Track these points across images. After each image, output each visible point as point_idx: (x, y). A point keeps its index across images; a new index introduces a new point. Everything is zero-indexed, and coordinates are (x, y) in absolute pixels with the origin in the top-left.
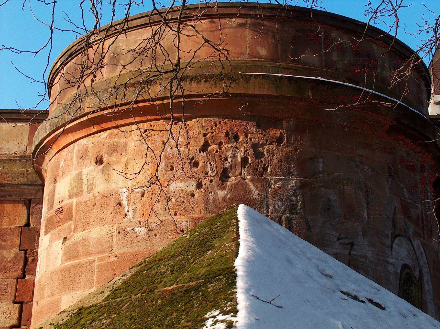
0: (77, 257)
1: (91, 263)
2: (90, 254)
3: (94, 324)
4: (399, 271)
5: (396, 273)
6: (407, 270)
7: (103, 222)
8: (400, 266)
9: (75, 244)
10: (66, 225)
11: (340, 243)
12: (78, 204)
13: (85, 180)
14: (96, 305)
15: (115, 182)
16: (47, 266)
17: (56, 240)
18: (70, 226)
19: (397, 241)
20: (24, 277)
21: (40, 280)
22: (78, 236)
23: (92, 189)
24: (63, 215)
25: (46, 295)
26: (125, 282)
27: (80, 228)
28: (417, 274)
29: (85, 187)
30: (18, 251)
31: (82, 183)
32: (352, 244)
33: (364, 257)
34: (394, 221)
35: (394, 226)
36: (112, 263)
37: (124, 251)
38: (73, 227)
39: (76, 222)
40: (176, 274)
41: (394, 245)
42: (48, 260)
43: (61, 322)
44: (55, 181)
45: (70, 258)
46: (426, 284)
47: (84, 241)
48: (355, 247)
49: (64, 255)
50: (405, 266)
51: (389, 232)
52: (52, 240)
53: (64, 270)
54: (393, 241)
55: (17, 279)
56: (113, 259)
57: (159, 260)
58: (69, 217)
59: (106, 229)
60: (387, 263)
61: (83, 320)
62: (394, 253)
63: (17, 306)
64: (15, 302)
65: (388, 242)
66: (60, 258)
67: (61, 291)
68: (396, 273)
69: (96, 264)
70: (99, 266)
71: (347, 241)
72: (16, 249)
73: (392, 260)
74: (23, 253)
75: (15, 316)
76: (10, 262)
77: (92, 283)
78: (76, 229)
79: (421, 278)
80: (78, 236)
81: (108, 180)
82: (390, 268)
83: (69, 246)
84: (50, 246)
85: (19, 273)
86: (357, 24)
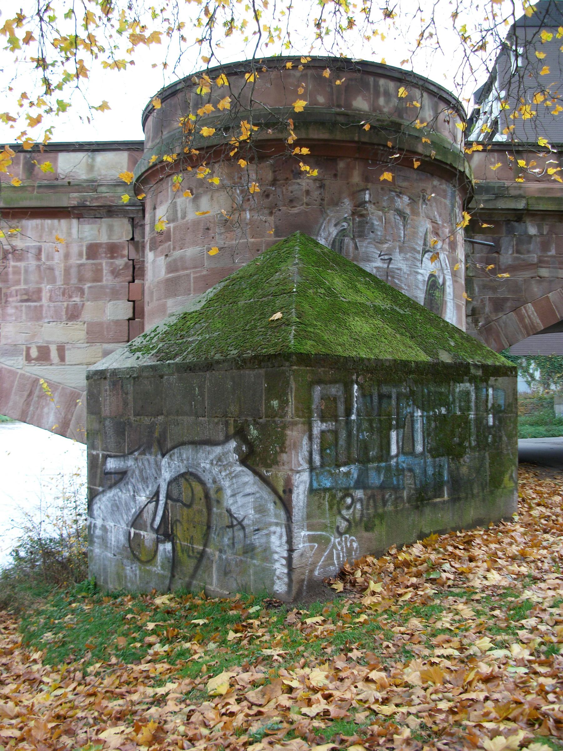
0: (177, 270)
1: (188, 275)
2: (187, 269)
3: (196, 326)
4: (426, 279)
5: (424, 281)
6: (433, 278)
7: (195, 243)
8: (428, 275)
9: (175, 260)
10: (167, 245)
11: (382, 259)
12: (175, 228)
13: (179, 209)
14: (196, 312)
15: (165, 65)
16: (154, 276)
17: (159, 256)
18: (169, 246)
19: (426, 255)
20: (133, 281)
21: (149, 287)
22: (177, 253)
23: (185, 216)
24: (163, 236)
25: (155, 298)
26: (216, 295)
27: (177, 248)
28: (441, 281)
29: (179, 215)
30: (127, 260)
31: (176, 211)
32: (390, 259)
33: (400, 269)
34: (425, 240)
35: (425, 244)
36: (204, 276)
37: (213, 266)
38: (172, 247)
39: (174, 242)
40: (254, 290)
41: (424, 259)
42: (154, 271)
43: (172, 324)
44: (155, 208)
45: (172, 272)
46: (447, 288)
47: (182, 258)
48: (392, 261)
49: (167, 268)
50: (432, 276)
51: (420, 249)
52: (156, 256)
53: (167, 280)
54: (423, 256)
55: (129, 282)
56: (205, 273)
57: (241, 278)
58: (168, 239)
59: (198, 249)
60: (417, 273)
61: (188, 323)
62: (423, 265)
63: (132, 303)
64: (129, 301)
65: (419, 257)
66: (163, 271)
67: (166, 297)
68: (424, 281)
69: (192, 276)
70: (194, 278)
71: (386, 257)
72: (126, 259)
73: (420, 271)
74: (131, 262)
75: (131, 311)
76: (122, 269)
77: (190, 291)
78: (174, 249)
79: (444, 284)
80: (177, 253)
81: (198, 208)
82: (420, 277)
83: (170, 262)
84: (154, 261)
85: (130, 278)
86: (401, 72)
